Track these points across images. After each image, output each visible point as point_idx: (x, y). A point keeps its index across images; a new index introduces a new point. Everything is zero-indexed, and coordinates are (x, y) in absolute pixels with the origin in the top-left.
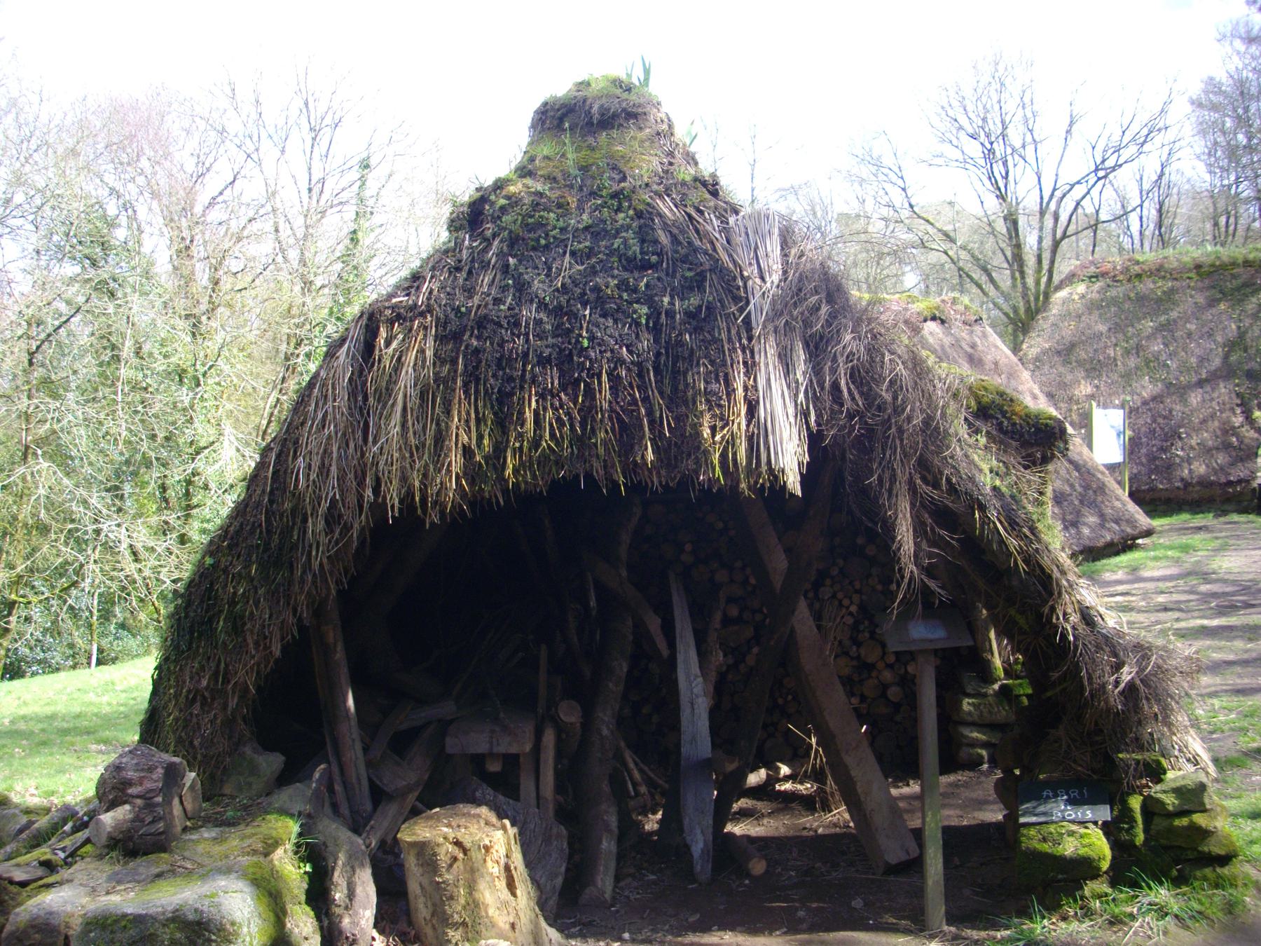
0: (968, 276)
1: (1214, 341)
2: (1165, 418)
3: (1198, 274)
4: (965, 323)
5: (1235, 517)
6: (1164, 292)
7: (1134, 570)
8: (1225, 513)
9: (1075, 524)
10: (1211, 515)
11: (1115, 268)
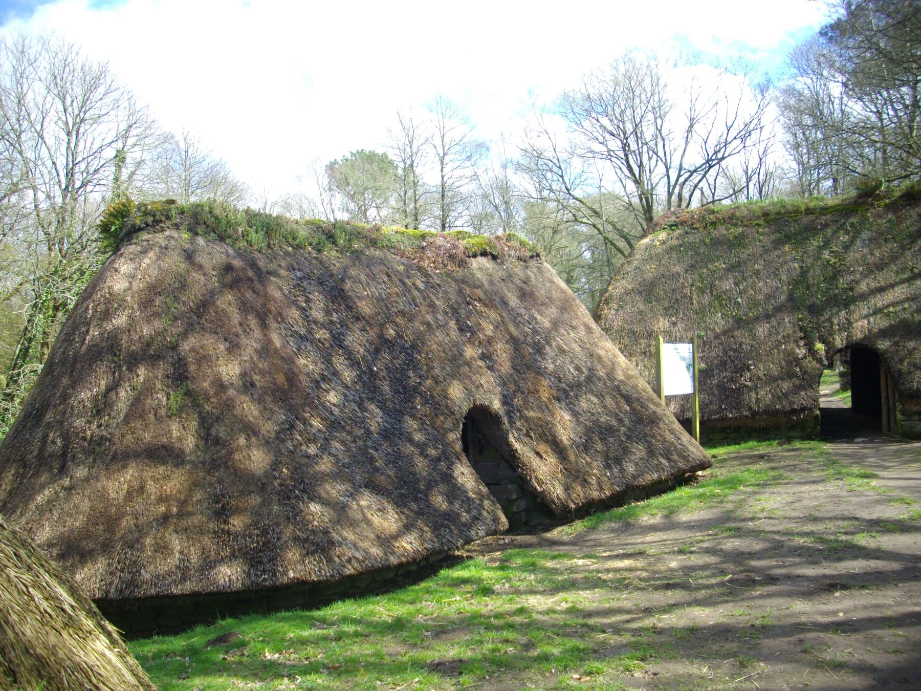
0: (612, 244)
2: (735, 351)
3: (765, 221)
4: (519, 259)
5: (797, 444)
6: (735, 237)
7: (671, 512)
8: (789, 440)
9: (618, 461)
10: (775, 443)
11: (692, 217)
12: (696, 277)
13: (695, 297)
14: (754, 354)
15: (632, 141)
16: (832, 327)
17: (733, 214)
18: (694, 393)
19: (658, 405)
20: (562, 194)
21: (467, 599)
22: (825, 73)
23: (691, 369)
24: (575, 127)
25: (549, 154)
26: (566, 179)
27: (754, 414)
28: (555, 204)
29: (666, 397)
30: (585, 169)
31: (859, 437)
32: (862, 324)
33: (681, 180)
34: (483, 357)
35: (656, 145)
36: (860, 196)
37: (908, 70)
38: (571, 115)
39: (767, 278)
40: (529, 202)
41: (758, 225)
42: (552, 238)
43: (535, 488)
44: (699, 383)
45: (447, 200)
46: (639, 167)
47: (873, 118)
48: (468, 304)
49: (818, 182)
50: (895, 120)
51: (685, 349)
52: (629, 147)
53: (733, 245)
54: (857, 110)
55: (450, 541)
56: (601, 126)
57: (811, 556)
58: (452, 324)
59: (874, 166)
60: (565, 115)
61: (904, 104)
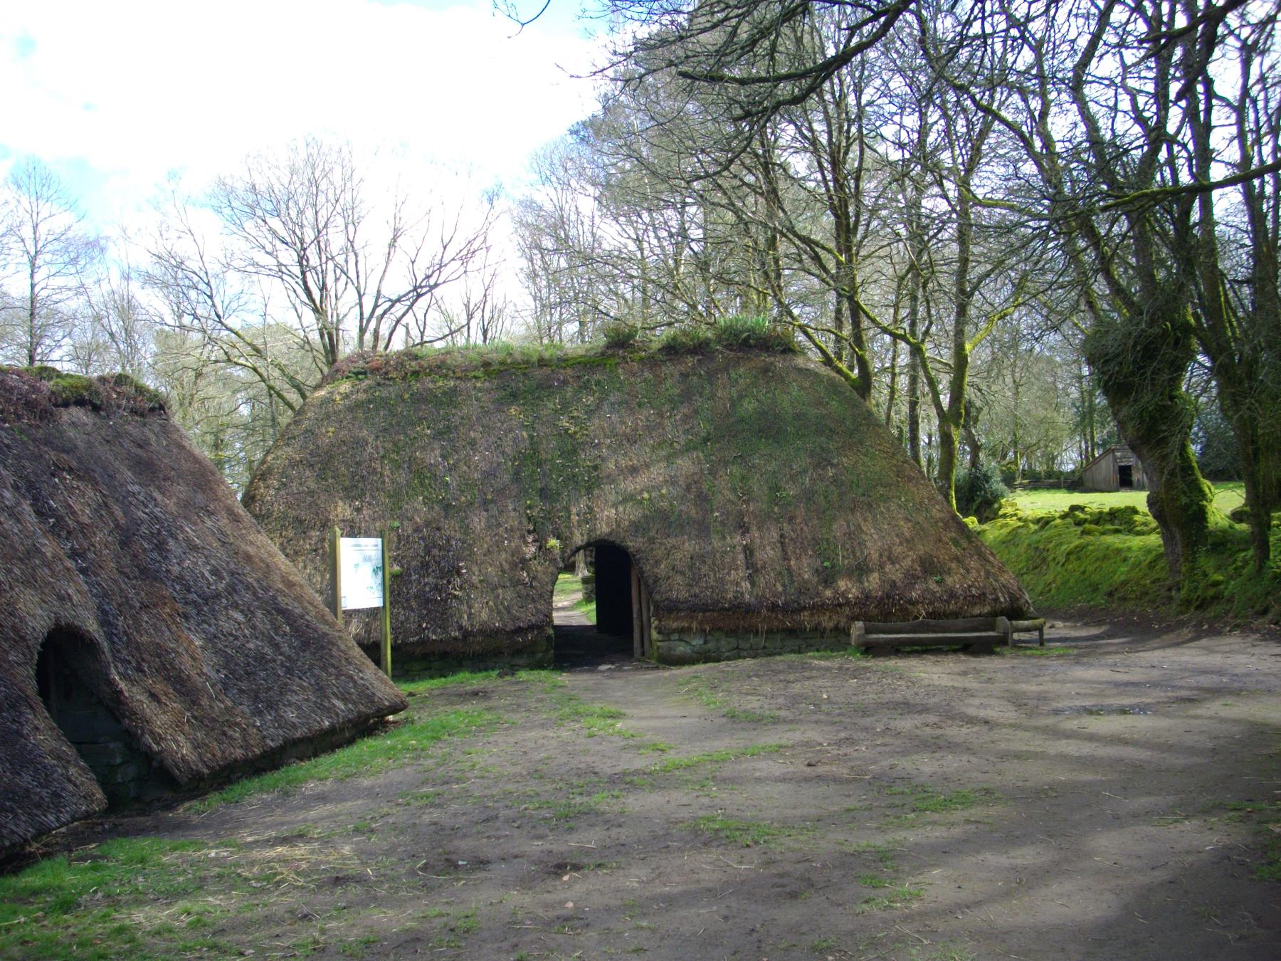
0: (280, 396)
1: (503, 453)
3: (486, 373)
5: (523, 675)
6: (444, 393)
8: (513, 669)
10: (494, 674)
11: (387, 363)
12: (389, 445)
13: (387, 472)
14: (467, 553)
15: (312, 253)
16: (569, 517)
17: (443, 362)
18: (384, 607)
19: (332, 625)
20: (210, 322)
21: (36, 920)
22: (573, 183)
23: (380, 573)
24: (234, 228)
25: (193, 264)
26: (217, 301)
27: (466, 634)
28: (200, 335)
29: (344, 612)
30: (246, 288)
31: (605, 663)
32: (609, 516)
33: (379, 311)
34: (74, 555)
35: (346, 261)
36: (609, 346)
37: (673, 190)
38: (227, 211)
39: (486, 449)
40: (162, 331)
41: (476, 377)
42: (195, 383)
43: (150, 747)
44: (391, 592)
45: (38, 322)
46: (321, 290)
47: (632, 246)
48: (53, 475)
49: (560, 324)
50: (657, 251)
51: (370, 547)
52: (308, 260)
53: (442, 403)
54: (614, 236)
55: (13, 832)
56: (270, 229)
57: (534, 827)
58: (26, 506)
59: (630, 308)
60: (218, 210)
61: (669, 232)
